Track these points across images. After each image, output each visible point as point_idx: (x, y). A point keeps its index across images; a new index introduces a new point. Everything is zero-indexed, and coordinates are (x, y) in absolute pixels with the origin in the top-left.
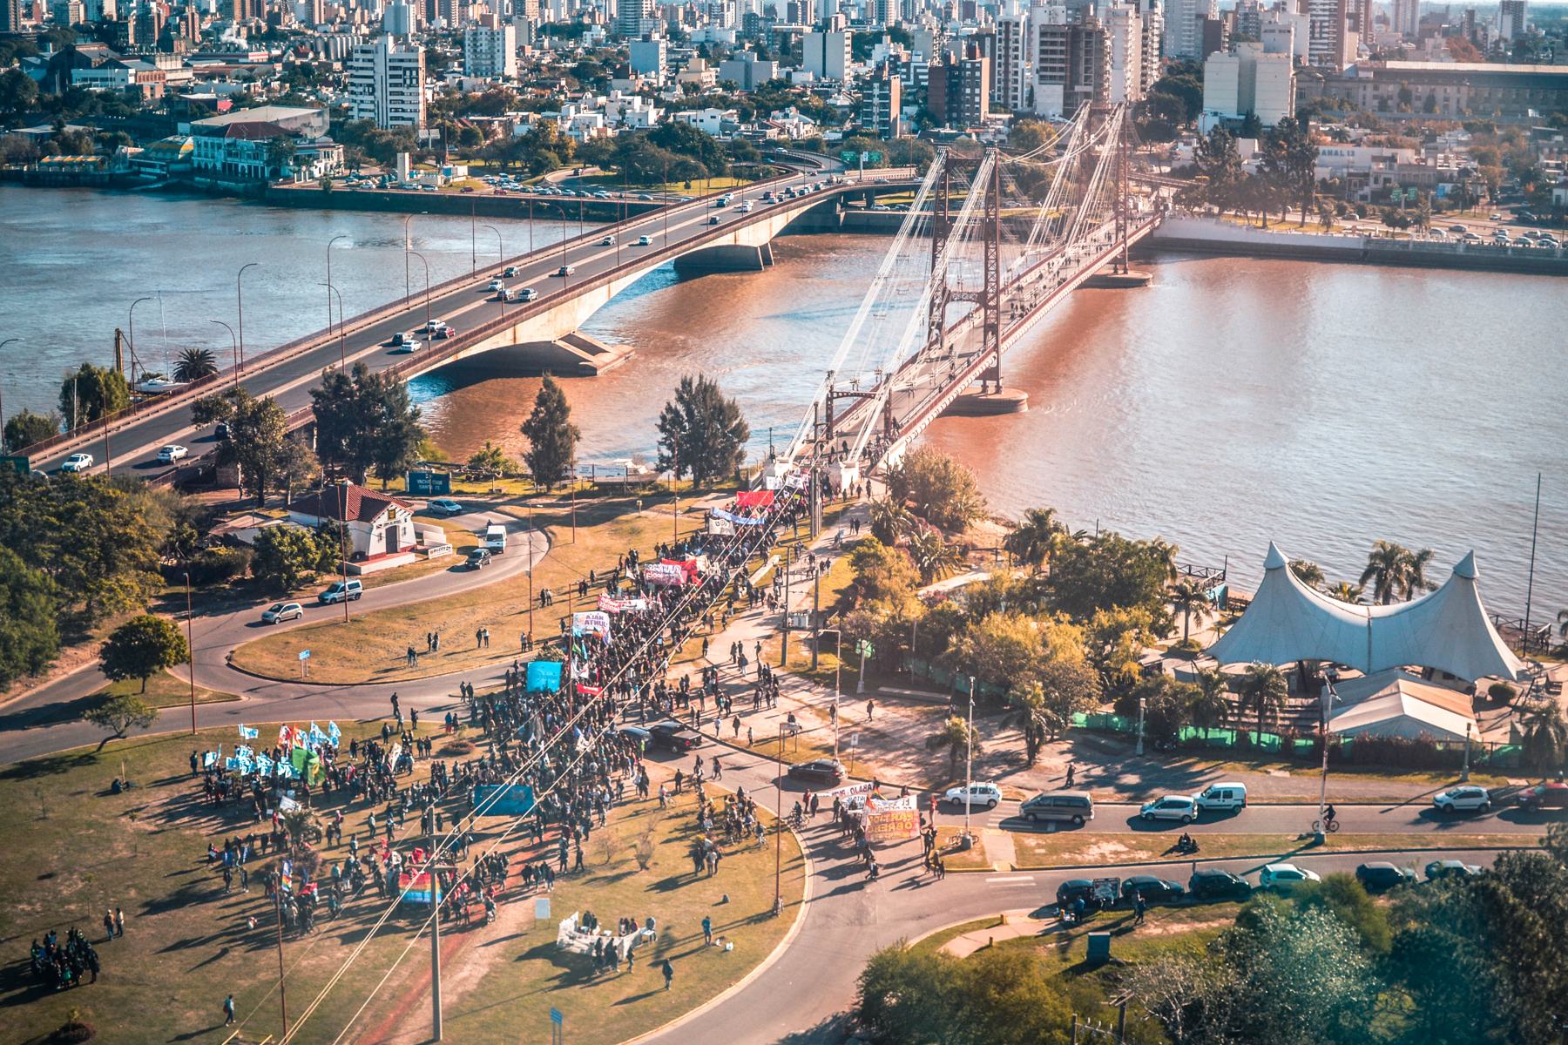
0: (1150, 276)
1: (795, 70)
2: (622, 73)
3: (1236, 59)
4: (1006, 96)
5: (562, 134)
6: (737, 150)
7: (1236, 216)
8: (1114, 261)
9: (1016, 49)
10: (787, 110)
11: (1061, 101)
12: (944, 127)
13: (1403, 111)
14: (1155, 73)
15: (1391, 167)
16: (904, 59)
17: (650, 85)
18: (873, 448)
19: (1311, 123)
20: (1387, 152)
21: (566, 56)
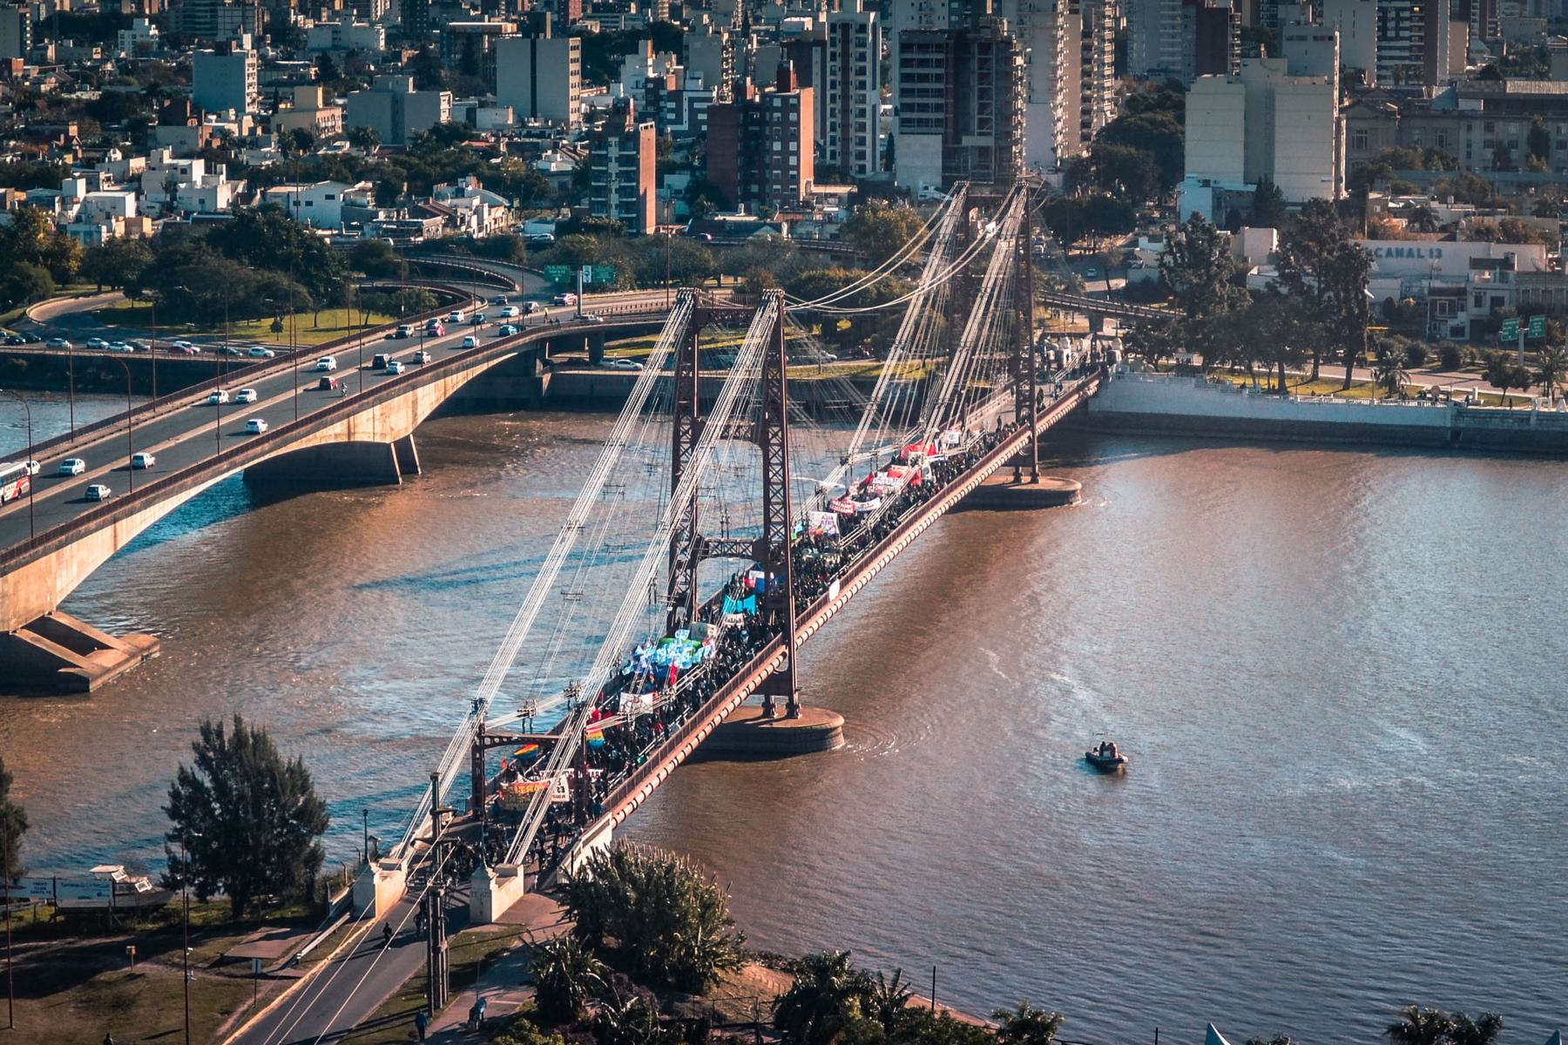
0: (1078, 486)
1: (482, 105)
2: (173, 117)
3: (1240, 88)
4: (845, 153)
5: (61, 229)
6: (366, 258)
7: (1232, 372)
8: (1015, 461)
9: (862, 71)
10: (461, 183)
11: (939, 163)
12: (735, 210)
13: (1534, 169)
14: (1107, 106)
15: (1503, 278)
16: (671, 86)
17: (225, 134)
18: (687, 707)
19: (1372, 196)
20: (1497, 251)
21: (87, 77)
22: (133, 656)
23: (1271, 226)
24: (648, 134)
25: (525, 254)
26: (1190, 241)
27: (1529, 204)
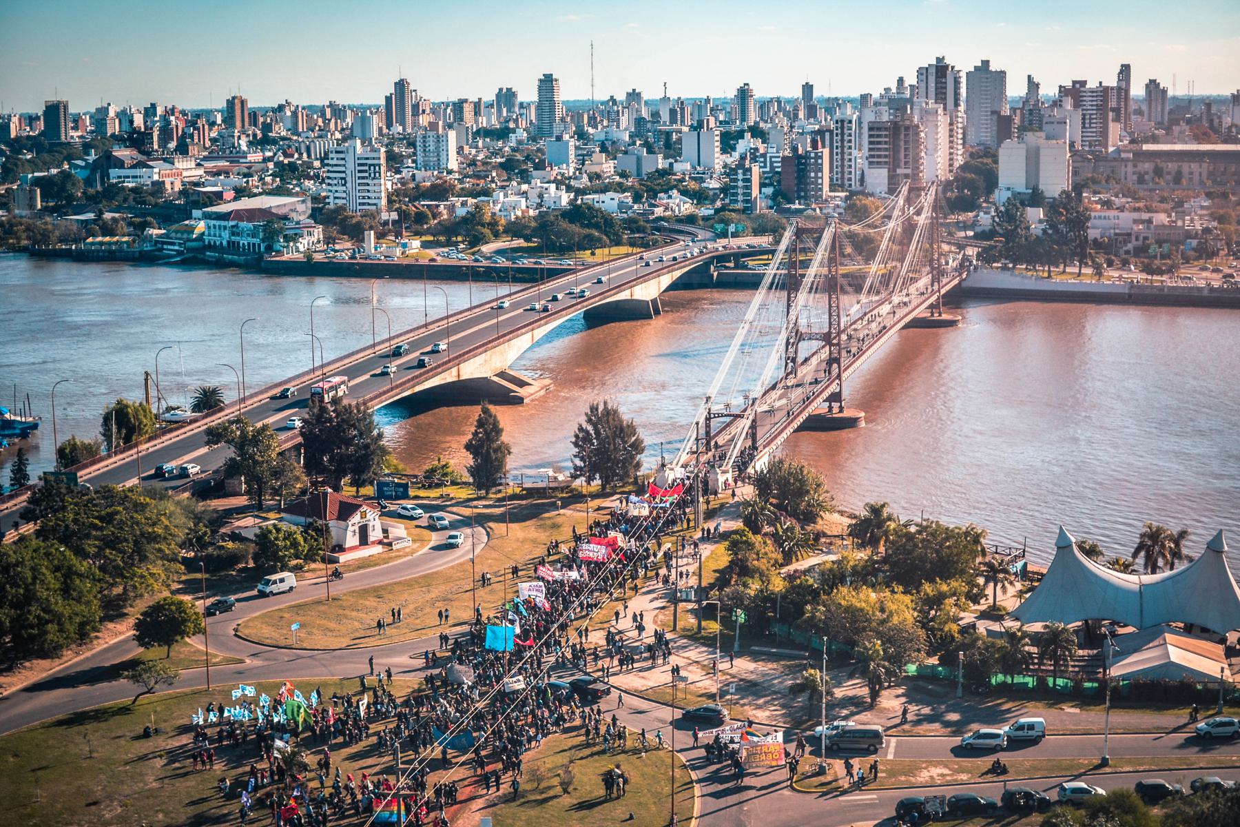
1: (676, 161)
3: (1023, 146)
4: (842, 178)
5: (494, 214)
8: (931, 307)
10: (670, 193)
11: (886, 181)
12: (794, 203)
13: (1157, 183)
14: (960, 158)
15: (1148, 228)
16: (762, 151)
19: (1084, 195)
20: (1145, 216)
21: (495, 153)
22: (542, 388)
23: (1038, 206)
24: (756, 170)
25: (701, 223)
26: (1007, 210)
27: (1157, 198)
